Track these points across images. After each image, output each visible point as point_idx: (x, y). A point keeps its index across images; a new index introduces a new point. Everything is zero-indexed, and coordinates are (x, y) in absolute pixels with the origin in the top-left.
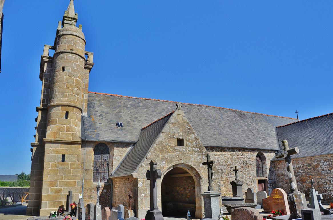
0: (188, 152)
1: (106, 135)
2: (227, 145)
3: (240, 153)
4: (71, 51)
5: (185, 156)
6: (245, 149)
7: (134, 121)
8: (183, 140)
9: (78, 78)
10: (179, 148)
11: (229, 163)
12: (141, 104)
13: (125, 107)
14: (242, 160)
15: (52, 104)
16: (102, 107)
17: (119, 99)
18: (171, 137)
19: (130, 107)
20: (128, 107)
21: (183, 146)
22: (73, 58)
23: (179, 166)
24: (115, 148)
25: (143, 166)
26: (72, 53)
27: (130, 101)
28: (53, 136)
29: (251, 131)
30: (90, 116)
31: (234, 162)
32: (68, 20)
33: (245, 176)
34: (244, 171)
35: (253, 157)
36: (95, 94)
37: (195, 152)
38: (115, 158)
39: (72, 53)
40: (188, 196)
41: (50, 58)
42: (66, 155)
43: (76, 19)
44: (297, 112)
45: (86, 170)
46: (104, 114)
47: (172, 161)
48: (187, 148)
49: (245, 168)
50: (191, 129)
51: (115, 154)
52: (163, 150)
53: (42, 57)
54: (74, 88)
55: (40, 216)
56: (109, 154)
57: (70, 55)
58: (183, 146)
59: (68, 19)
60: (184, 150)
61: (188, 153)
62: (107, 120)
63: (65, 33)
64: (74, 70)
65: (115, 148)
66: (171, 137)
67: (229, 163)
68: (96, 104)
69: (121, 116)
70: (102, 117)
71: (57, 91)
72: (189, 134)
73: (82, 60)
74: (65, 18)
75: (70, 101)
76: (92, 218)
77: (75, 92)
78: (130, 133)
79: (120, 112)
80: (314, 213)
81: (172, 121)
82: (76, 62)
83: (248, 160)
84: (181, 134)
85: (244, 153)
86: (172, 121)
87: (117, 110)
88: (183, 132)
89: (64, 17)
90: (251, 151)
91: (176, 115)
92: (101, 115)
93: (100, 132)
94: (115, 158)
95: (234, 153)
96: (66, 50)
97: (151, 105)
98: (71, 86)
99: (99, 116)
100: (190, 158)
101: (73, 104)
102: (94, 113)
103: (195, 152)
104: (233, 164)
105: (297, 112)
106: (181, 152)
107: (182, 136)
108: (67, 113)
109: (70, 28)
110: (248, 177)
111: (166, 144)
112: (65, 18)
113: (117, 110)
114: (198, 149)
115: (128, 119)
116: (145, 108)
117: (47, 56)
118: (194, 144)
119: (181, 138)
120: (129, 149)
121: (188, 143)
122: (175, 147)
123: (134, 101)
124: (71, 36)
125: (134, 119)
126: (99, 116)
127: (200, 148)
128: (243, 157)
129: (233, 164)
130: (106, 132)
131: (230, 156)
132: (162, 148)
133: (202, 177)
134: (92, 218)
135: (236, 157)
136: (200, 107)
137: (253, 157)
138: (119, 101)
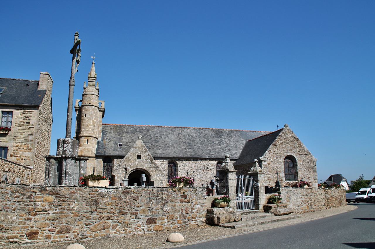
0: (143, 162)
1: (110, 152)
2: (191, 156)
3: (202, 162)
4: (89, 104)
5: (141, 164)
6: (206, 159)
7: (130, 142)
8: (141, 156)
9: (94, 120)
10: (138, 160)
12: (138, 130)
13: (127, 133)
14: (203, 166)
15: (81, 135)
16: (112, 134)
17: (124, 127)
18: (133, 155)
19: (130, 133)
20: (129, 133)
21: (141, 159)
22: (90, 108)
23: (138, 170)
24: (114, 159)
25: (118, 169)
26: (90, 105)
27: (131, 128)
28: (80, 154)
29: (220, 145)
30: (103, 140)
31: (196, 167)
32: (91, 79)
33: (205, 177)
34: (204, 173)
35: (213, 164)
36: (109, 125)
37: (148, 162)
38: (115, 165)
39: (90, 105)
40: (261, 210)
41: (79, 107)
43: (96, 78)
44: (278, 127)
46: (112, 138)
47: (133, 167)
48: (143, 160)
49: (206, 171)
50: (146, 150)
51: (114, 162)
52: (129, 161)
53: (75, 107)
54: (92, 126)
56: (112, 162)
57: (89, 106)
58: (141, 159)
59: (90, 78)
60: (141, 161)
62: (113, 142)
63: (86, 93)
64: (91, 115)
65: (114, 159)
66: (133, 155)
68: (108, 131)
69: (122, 139)
70: (111, 140)
71: (82, 128)
72: (145, 152)
73: (96, 108)
74: (89, 78)
75: (89, 134)
76: (1, 132)
77: (92, 128)
78: (125, 150)
79: (122, 136)
81: (135, 146)
82: (93, 110)
83: (209, 166)
84: (140, 153)
85: (206, 161)
86: (135, 146)
87: (121, 135)
88: (141, 152)
89: (88, 77)
90: (211, 160)
91: (137, 143)
92: (110, 139)
93: (107, 150)
94: (115, 165)
95: (197, 162)
96: (87, 104)
97: (145, 130)
98: (90, 125)
99: (109, 140)
100: (144, 165)
101: (91, 135)
102: (106, 138)
103: (148, 162)
104: (196, 169)
105: (278, 127)
108: (88, 140)
109: (89, 89)
110: (208, 178)
111: (131, 158)
112: (89, 78)
113: (121, 135)
114: (150, 161)
115: (127, 141)
116: (140, 133)
117: (78, 106)
118: (148, 158)
121: (144, 157)
123: (134, 128)
124: (89, 95)
125: (130, 141)
126: (109, 140)
127: (151, 160)
128: (204, 164)
129: (196, 169)
130: (111, 150)
131: (193, 164)
133: (151, 175)
134: (1, 132)
135: (199, 164)
136: (183, 129)
137: (213, 164)
138: (123, 128)
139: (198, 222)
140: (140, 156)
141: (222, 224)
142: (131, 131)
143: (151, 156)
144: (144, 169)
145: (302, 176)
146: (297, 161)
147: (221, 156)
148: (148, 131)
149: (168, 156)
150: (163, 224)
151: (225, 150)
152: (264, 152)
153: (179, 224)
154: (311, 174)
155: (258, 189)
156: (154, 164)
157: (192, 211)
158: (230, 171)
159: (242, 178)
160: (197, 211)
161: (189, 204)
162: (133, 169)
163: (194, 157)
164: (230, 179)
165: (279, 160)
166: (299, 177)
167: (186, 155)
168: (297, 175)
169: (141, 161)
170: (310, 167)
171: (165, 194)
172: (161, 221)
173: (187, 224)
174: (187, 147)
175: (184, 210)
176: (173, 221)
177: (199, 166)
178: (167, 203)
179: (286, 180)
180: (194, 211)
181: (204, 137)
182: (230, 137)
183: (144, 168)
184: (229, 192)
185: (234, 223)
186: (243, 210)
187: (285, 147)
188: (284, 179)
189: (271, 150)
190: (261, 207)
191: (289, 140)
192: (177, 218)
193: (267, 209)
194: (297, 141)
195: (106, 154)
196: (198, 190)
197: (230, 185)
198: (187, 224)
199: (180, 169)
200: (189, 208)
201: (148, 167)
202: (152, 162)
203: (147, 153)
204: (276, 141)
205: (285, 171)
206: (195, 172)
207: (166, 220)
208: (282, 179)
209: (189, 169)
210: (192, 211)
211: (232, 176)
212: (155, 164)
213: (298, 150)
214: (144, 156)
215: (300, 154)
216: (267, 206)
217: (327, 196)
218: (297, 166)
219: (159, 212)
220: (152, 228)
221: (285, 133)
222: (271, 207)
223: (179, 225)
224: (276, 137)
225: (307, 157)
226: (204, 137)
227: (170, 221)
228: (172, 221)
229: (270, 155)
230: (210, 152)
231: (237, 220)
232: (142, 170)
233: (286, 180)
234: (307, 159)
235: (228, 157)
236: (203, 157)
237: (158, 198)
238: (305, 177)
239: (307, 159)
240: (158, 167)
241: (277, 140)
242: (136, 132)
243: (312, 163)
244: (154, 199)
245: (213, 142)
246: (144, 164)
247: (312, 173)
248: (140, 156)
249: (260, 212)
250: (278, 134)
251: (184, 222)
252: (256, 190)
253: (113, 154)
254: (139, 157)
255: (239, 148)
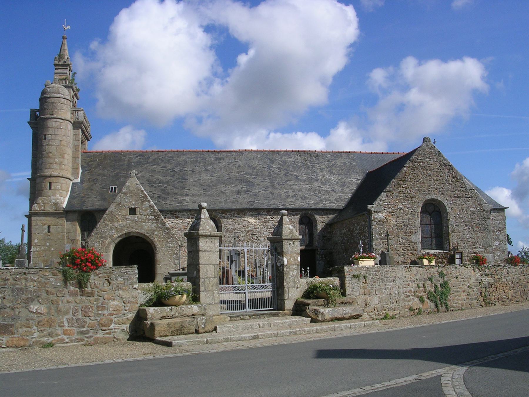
2: (248, 206)
8: (135, 209)
10: (130, 217)
11: (249, 229)
40: (288, 310)
42: (51, 227)
45: (71, 240)
52: (113, 220)
55: (117, 271)
60: (136, 218)
61: (141, 221)
67: (249, 229)
72: (143, 202)
80: (143, 345)
81: (124, 191)
84: (134, 203)
86: (124, 191)
88: (136, 201)
103: (149, 220)
106: (132, 221)
107: (135, 204)
114: (153, 217)
118: (149, 211)
119: (133, 207)
120: (331, 217)
122: (126, 216)
127: (155, 216)
129: (257, 230)
132: (112, 217)
139: (115, 332)
140: (135, 209)
141: (161, 336)
142: (137, 162)
143: (156, 208)
144: (142, 234)
145: (458, 241)
146: (449, 209)
147: (309, 204)
148: (169, 161)
149: (328, 206)
150: (27, 336)
151: (319, 192)
152: (379, 194)
153: (68, 336)
154: (478, 237)
155: (283, 270)
156: (162, 224)
157: (100, 312)
158: (202, 236)
159: (246, 249)
160: (112, 312)
161: (92, 298)
162: (121, 234)
163: (252, 207)
164: (202, 251)
165: (408, 210)
166: (451, 243)
167: (239, 205)
168: (449, 239)
169: (136, 218)
170: (477, 222)
171: (32, 280)
172: (25, 329)
173: (87, 335)
174: (242, 188)
175: (80, 310)
176: (53, 330)
177: (264, 224)
178: (38, 296)
179: (423, 248)
180: (105, 312)
181: (279, 168)
182: (333, 165)
183: (142, 231)
184: (201, 276)
185: (196, 335)
186: (245, 310)
187: (424, 183)
188: (420, 246)
189: (392, 189)
190: (289, 305)
191: (431, 170)
192: (62, 325)
193: (299, 310)
194: (450, 170)
195: (84, 208)
196: (115, 273)
197: (201, 261)
198: (87, 335)
199: (226, 232)
200: (92, 307)
201: (150, 229)
202: (157, 220)
203: (147, 203)
204: (404, 172)
205: (422, 231)
206: (255, 237)
207: (35, 328)
208: (415, 246)
209: (243, 230)
210: (100, 312)
211: (208, 245)
212: (164, 224)
213: (450, 188)
214: (142, 209)
215: (456, 197)
216: (302, 302)
217: (486, 280)
218: (448, 220)
219: (19, 312)
220: (5, 341)
221: (424, 154)
222: (308, 305)
223: (67, 338)
224: (405, 163)
225: (470, 203)
226: (279, 168)
227: (44, 330)
228: (49, 330)
229: (390, 199)
230: (288, 197)
231: (201, 330)
232: (140, 236)
233: (423, 248)
234: (470, 206)
235: (203, 208)
236: (272, 207)
237: (16, 288)
238: (465, 242)
239: (470, 206)
240: (168, 229)
241: (405, 169)
242: (146, 164)
243: (482, 214)
244: (6, 289)
245: (297, 177)
246: (143, 225)
247: (479, 235)
248: (135, 209)
249: (285, 315)
250: (409, 159)
251: (82, 333)
252: (279, 270)
253: (97, 207)
254: (133, 211)
255: (348, 187)
